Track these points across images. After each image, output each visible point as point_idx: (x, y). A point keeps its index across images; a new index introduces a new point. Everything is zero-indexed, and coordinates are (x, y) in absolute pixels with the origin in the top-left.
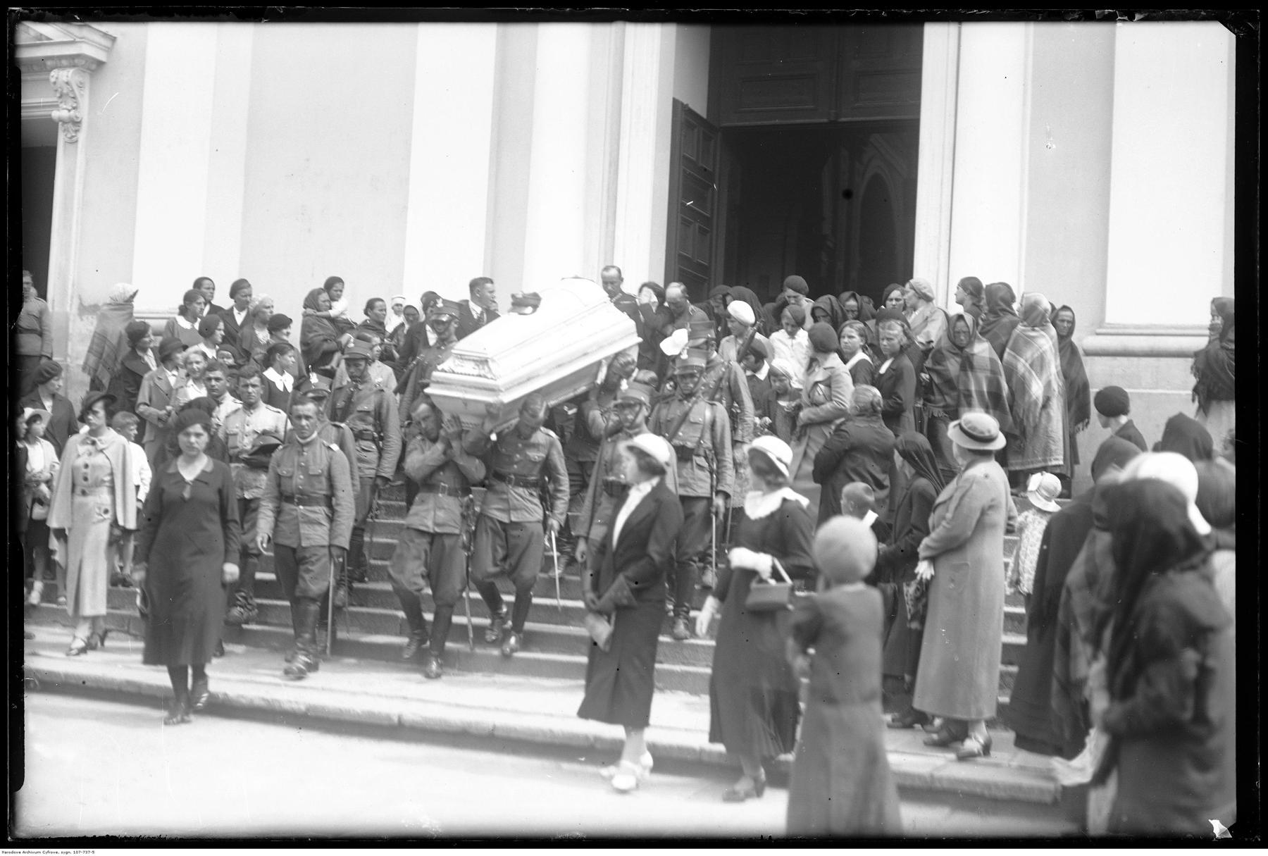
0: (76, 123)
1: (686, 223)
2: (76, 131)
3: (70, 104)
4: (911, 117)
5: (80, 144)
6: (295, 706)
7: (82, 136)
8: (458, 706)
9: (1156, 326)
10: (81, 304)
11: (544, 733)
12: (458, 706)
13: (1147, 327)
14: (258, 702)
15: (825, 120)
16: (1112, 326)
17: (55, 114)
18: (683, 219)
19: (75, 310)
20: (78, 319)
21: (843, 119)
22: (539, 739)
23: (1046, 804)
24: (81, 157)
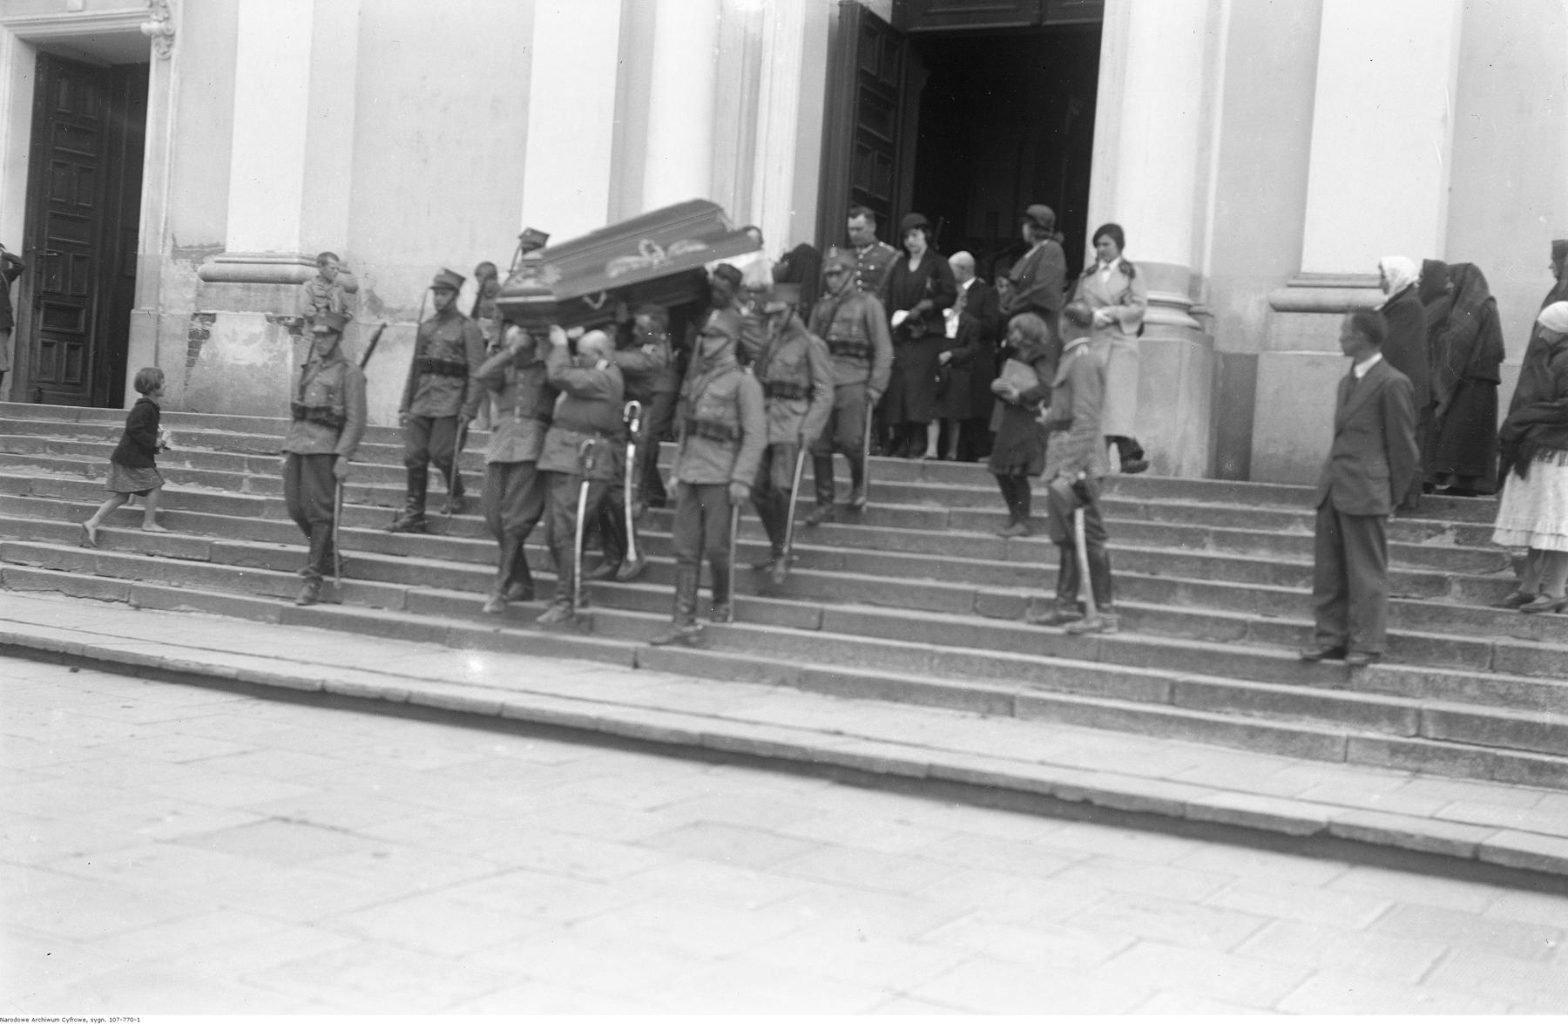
0: (170, 37)
1: (862, 151)
2: (169, 46)
3: (162, 14)
4: (1094, 20)
5: (173, 60)
6: (227, 671)
7: (175, 52)
8: (867, 739)
9: (1358, 277)
10: (175, 246)
11: (823, 752)
12: (867, 739)
13: (1349, 277)
14: (193, 667)
15: (1027, 23)
16: (1307, 276)
17: (146, 27)
18: (860, 147)
19: (168, 253)
20: (171, 263)
21: (1048, 22)
22: (451, 707)
23: (1462, 860)
24: (174, 77)
